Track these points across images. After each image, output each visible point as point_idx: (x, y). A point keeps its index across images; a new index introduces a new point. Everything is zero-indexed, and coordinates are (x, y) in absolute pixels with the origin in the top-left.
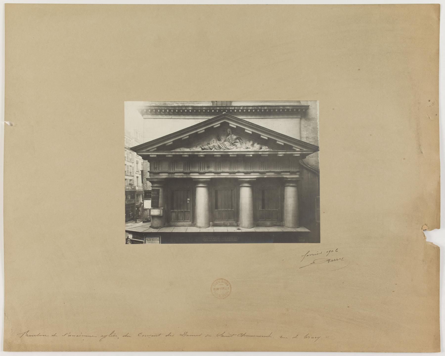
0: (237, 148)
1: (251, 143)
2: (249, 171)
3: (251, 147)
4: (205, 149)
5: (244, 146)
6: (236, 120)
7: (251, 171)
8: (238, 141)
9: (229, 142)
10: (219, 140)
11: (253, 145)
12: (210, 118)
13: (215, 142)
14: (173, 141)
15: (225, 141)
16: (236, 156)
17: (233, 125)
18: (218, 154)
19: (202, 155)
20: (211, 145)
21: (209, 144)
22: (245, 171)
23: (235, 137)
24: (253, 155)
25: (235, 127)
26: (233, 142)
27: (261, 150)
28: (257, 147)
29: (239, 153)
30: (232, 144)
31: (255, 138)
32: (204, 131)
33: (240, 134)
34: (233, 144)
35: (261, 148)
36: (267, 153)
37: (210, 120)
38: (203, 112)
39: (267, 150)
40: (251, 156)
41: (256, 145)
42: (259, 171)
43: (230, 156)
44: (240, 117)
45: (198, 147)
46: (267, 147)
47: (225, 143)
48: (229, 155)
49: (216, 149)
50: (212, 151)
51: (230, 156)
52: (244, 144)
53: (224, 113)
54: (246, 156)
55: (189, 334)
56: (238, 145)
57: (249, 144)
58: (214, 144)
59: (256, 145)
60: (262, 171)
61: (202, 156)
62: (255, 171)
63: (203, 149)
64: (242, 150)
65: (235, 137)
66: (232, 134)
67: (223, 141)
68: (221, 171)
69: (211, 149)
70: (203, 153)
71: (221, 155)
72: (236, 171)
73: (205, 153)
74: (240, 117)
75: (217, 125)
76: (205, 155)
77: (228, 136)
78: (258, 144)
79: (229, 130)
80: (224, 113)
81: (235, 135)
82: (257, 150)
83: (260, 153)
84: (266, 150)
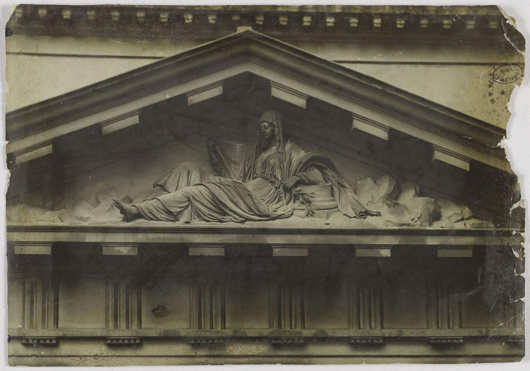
0: (311, 214)
1: (386, 186)
2: (377, 332)
3: (384, 209)
4: (139, 215)
5: (347, 200)
6: (323, 65)
7: (387, 333)
8: (315, 174)
9: (270, 179)
10: (219, 167)
11: (393, 199)
12: (168, 52)
13: (195, 177)
14: (143, 112)
15: (245, 177)
16: (305, 253)
17: (292, 92)
18: (207, 245)
19: (122, 245)
20: (172, 196)
21: (163, 188)
22: (353, 332)
23: (298, 156)
24: (394, 248)
25: (301, 102)
26: (290, 182)
27: (436, 226)
28: (414, 208)
29: (321, 239)
30: (287, 190)
31: (401, 162)
32: (135, 120)
33: (327, 140)
34: (292, 192)
35: (436, 216)
36: (468, 240)
37: (162, 64)
38: (326, 29)
39: (469, 225)
40: (386, 253)
41: (408, 198)
42: (430, 333)
43: (277, 252)
44: (331, 55)
45: (106, 203)
46: (467, 212)
47: (250, 185)
48: (270, 247)
49: (200, 216)
50: (180, 224)
51: (277, 252)
52: (350, 194)
53: (241, 30)
54: (360, 253)
55: (369, 203)
56: (320, 197)
57: (373, 193)
58: (193, 190)
59: (408, 198)
60: (445, 332)
61: (124, 251)
62: (407, 333)
63: (128, 216)
64: (337, 221)
65: (298, 156)
66: (287, 137)
67: (236, 173)
68: (228, 332)
69: (175, 217)
70: (130, 238)
71: (226, 246)
72: (307, 333)
73: (141, 238)
74: (331, 55)
75: (205, 89)
76: (142, 247)
77: (265, 149)
78: (420, 194)
79: (268, 120)
80: (241, 30)
81: (299, 143)
82: (417, 225)
83: (431, 241)
84: (460, 226)
